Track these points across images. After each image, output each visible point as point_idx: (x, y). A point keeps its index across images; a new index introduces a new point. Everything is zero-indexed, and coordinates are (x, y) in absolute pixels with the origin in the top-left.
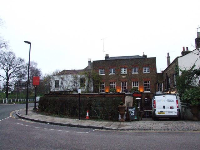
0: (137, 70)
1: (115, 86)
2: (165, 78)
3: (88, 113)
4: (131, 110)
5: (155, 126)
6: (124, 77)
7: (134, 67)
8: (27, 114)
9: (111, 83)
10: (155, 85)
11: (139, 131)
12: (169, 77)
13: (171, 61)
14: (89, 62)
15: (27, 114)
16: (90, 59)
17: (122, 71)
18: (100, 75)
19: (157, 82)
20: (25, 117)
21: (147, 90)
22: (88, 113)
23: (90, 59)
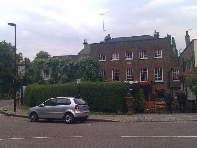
0: (132, 55)
1: (132, 74)
2: (181, 64)
3: (132, 90)
4: (131, 105)
5: (163, 118)
6: (129, 63)
7: (114, 52)
8: (15, 111)
9: (113, 71)
10: (169, 74)
11: (144, 123)
12: (186, 63)
13: (191, 40)
14: (85, 44)
15: (15, 111)
16: (86, 40)
17: (114, 57)
18: (100, 61)
19: (172, 69)
20: (14, 113)
21: (159, 78)
22: (132, 90)
23: (86, 40)
